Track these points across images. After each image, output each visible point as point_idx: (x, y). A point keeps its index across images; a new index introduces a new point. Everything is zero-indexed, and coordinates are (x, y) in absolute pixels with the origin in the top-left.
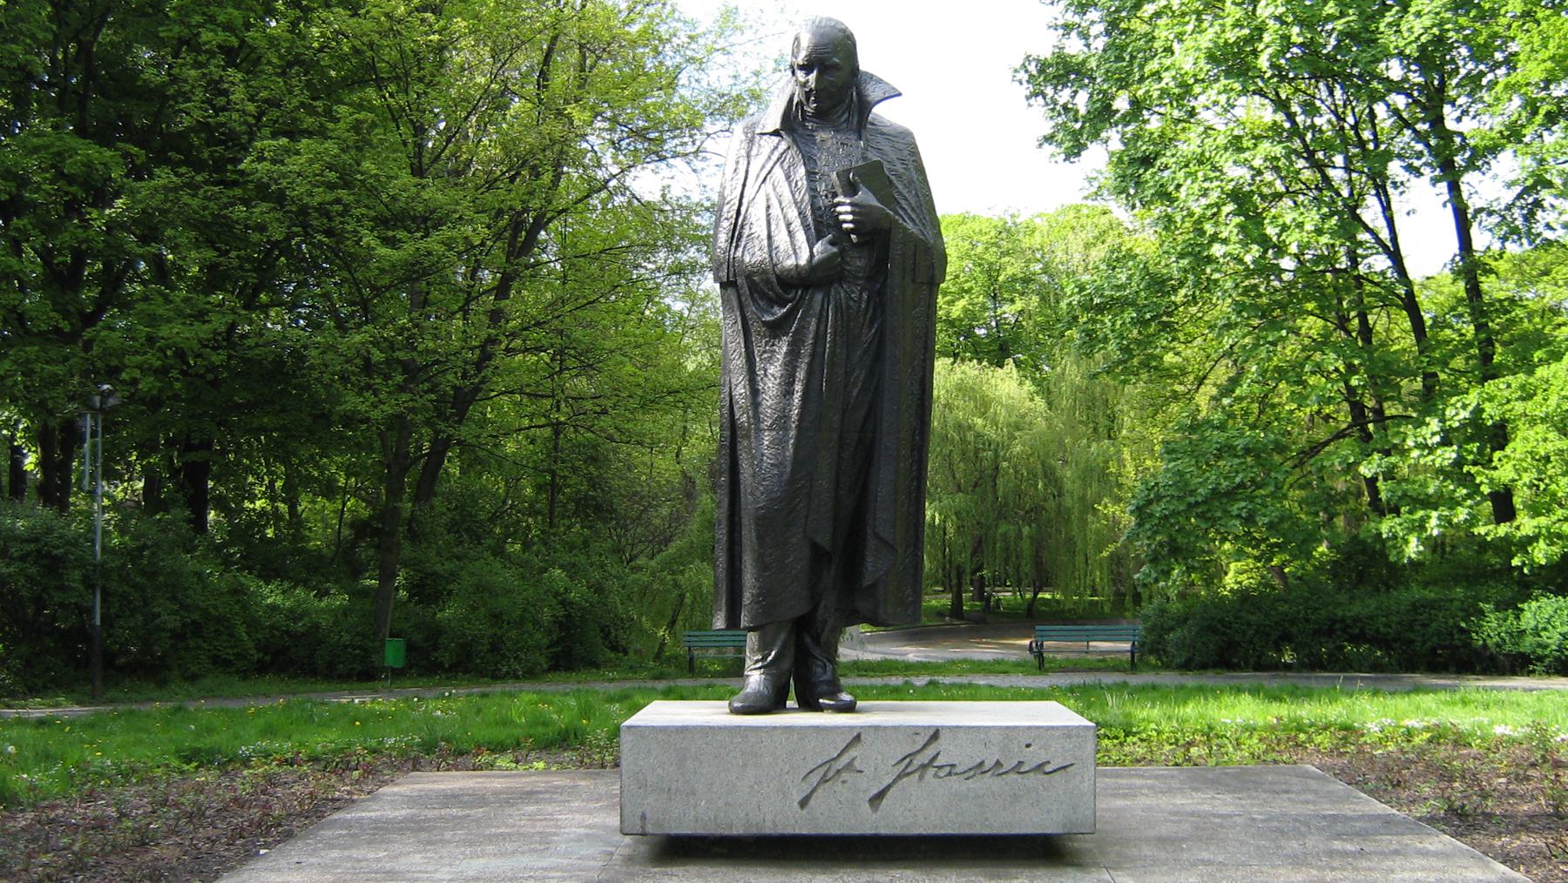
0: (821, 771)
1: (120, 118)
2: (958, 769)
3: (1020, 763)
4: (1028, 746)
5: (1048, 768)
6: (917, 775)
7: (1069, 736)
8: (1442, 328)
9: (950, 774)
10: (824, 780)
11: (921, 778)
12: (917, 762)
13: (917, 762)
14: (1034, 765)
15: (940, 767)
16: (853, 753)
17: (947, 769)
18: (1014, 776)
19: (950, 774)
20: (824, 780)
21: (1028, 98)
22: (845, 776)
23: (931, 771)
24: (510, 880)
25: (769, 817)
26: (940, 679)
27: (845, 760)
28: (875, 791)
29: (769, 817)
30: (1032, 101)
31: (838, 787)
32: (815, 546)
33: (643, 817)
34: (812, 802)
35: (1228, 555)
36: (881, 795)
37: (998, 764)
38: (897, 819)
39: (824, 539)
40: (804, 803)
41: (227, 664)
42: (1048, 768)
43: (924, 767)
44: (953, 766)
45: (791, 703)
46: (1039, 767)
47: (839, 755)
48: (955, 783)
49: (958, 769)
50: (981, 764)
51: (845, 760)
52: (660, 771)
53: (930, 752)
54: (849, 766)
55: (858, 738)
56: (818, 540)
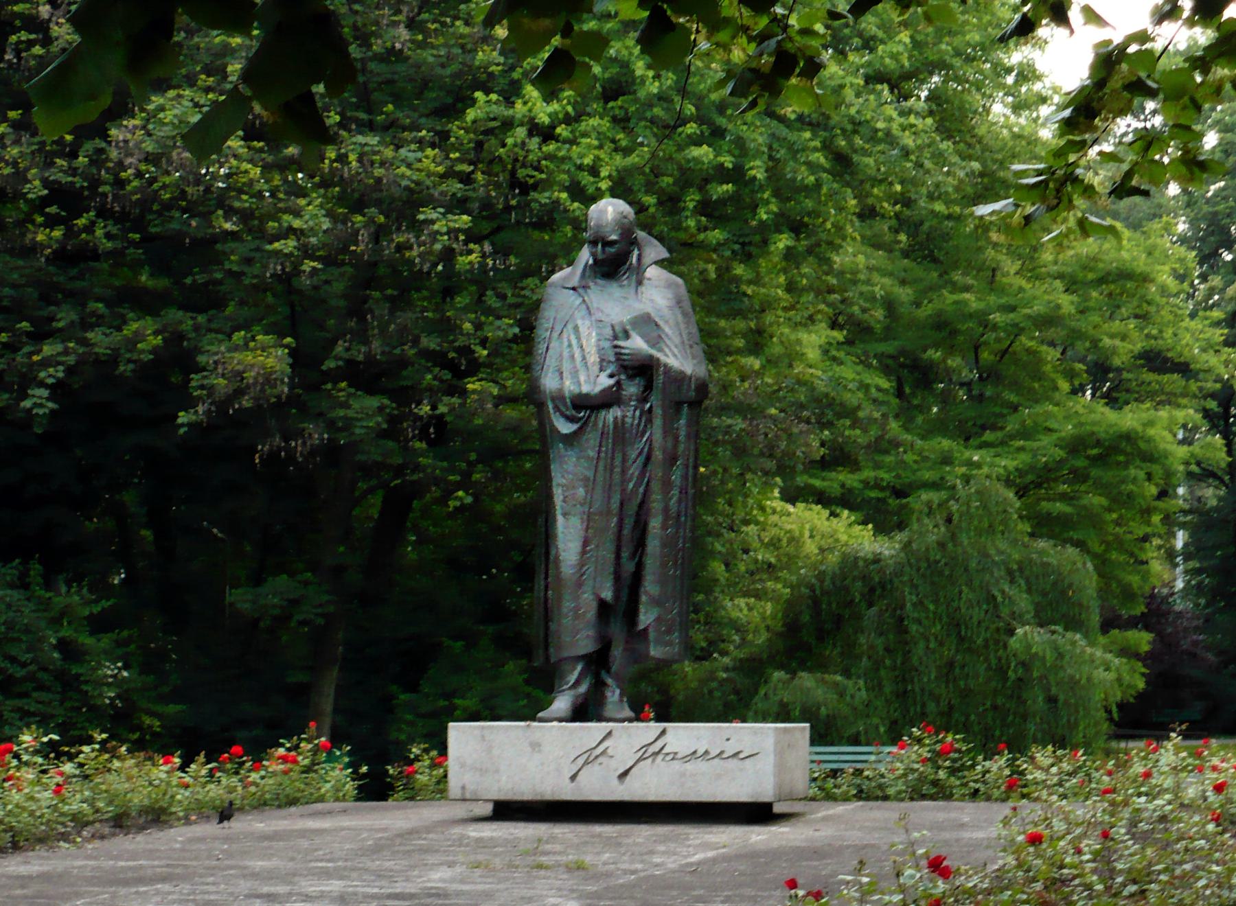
0: (586, 756)
2: (679, 756)
3: (722, 752)
5: (742, 756)
10: (586, 763)
11: (653, 761)
12: (652, 750)
13: (652, 750)
17: (671, 756)
20: (586, 763)
22: (600, 760)
23: (660, 757)
28: (621, 771)
33: (463, 788)
34: (578, 778)
37: (707, 752)
39: (607, 595)
40: (573, 778)
42: (742, 756)
43: (656, 754)
46: (736, 755)
49: (679, 756)
50: (695, 752)
53: (659, 744)
54: (604, 753)
55: (610, 733)
56: (603, 595)
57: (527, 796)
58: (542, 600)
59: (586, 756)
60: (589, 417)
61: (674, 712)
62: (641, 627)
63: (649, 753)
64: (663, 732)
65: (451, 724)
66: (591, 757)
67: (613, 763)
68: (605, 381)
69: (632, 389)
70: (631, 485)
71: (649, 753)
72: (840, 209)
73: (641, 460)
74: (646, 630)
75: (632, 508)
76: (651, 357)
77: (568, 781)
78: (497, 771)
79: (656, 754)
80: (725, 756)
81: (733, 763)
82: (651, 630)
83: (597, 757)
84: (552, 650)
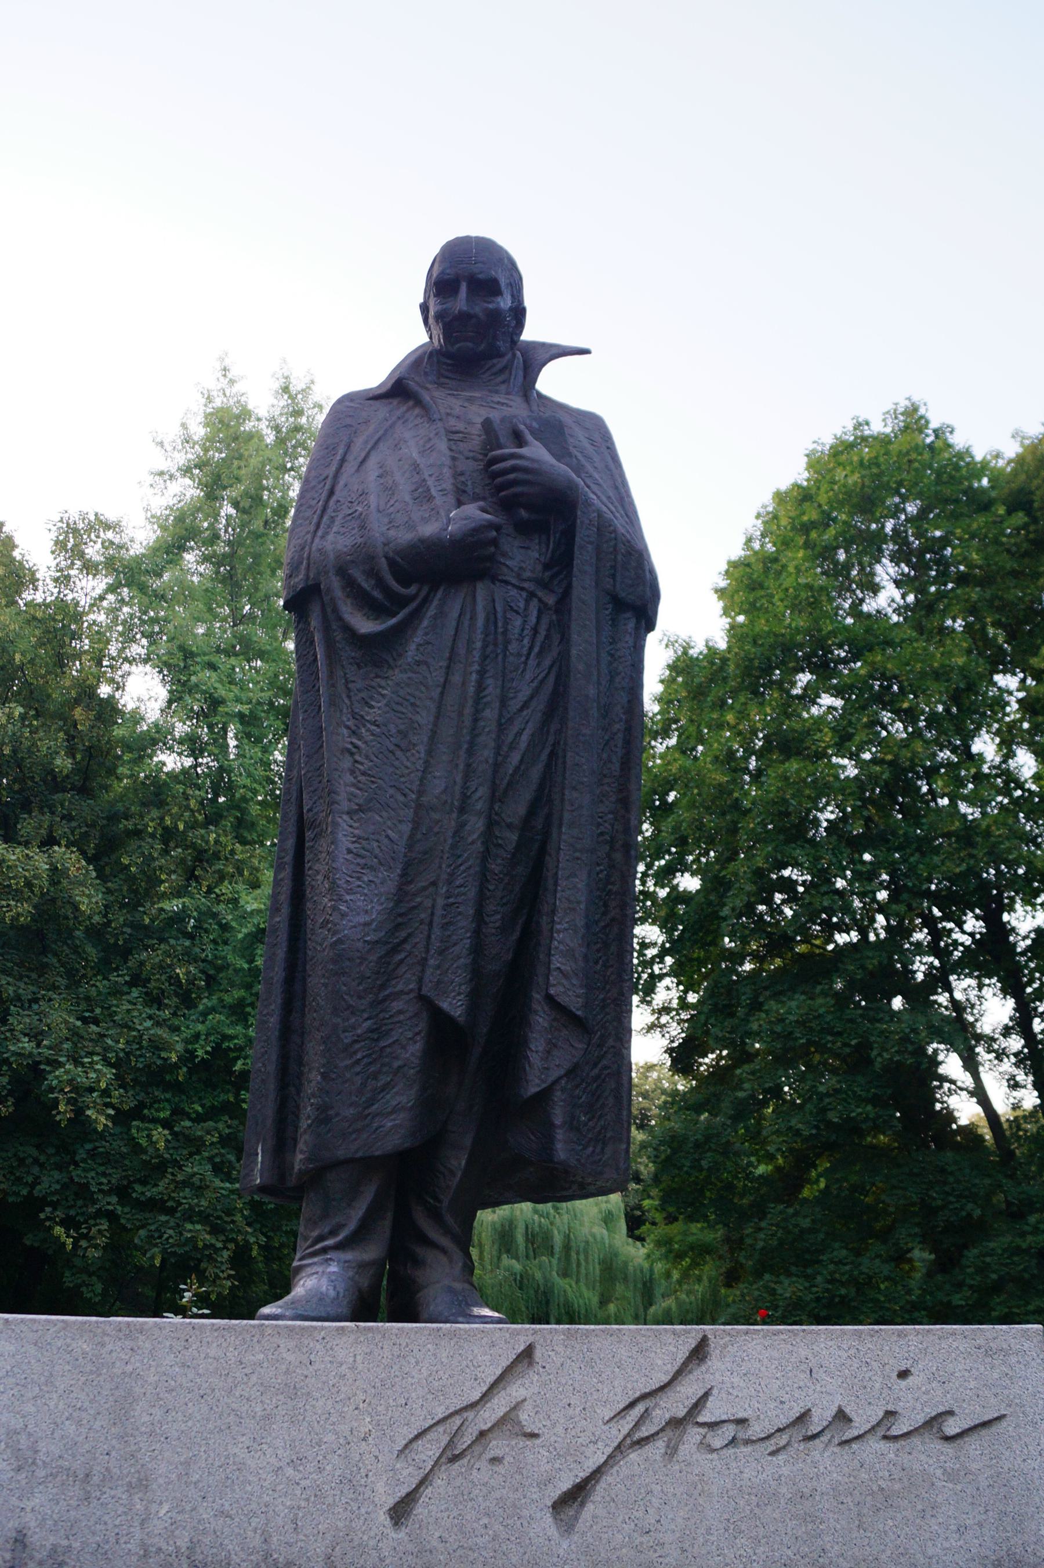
1: (1019, 533)
4: (903, 1374)
5: (952, 1427)
6: (660, 1445)
9: (733, 1442)
10: (451, 1456)
11: (671, 1451)
12: (674, 1404)
14: (920, 1419)
15: (712, 1426)
16: (516, 1391)
17: (729, 1431)
18: (875, 1445)
19: (733, 1442)
20: (451, 1456)
21: (313, 382)
22: (497, 1446)
23: (694, 1435)
26: (500, 630)
27: (498, 1406)
28: (565, 1484)
30: (307, 380)
31: (481, 1472)
32: (438, 1019)
34: (420, 1510)
35: (1021, 720)
36: (577, 1495)
37: (842, 1417)
39: (454, 1005)
43: (676, 1423)
44: (741, 1422)
46: (934, 1422)
47: (485, 1397)
48: (752, 1467)
49: (756, 1430)
50: (803, 1418)
51: (498, 1406)
52: (70, 1428)
53: (688, 1390)
60: (426, 601)
61: (554, 1313)
62: (533, 1088)
64: (699, 1353)
65: (426, 339)
67: (537, 1458)
69: (522, 558)
70: (515, 758)
73: (539, 705)
74: (544, 1096)
75: (516, 809)
76: (570, 481)
77: (383, 1518)
78: (142, 1484)
81: (928, 1455)
82: (558, 1095)
84: (391, 886)
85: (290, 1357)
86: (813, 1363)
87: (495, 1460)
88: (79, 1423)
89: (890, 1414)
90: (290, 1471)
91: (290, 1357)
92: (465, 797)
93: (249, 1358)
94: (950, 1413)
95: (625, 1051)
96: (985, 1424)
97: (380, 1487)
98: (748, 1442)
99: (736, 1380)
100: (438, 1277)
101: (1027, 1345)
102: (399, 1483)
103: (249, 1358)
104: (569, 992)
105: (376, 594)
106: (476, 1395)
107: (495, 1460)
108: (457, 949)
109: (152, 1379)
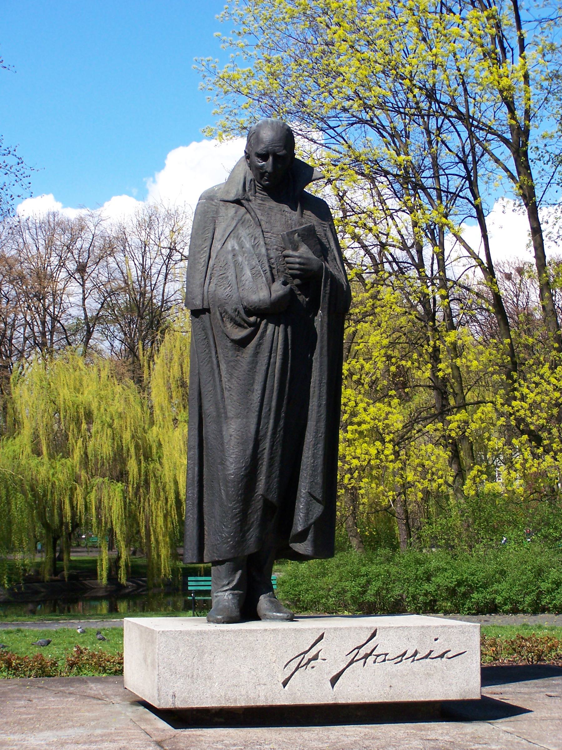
4: (436, 640)
5: (450, 655)
7: (463, 633)
8: (121, 587)
9: (384, 661)
12: (363, 652)
13: (363, 652)
15: (378, 656)
19: (384, 661)
23: (371, 659)
24: (5, 408)
25: (262, 694)
28: (335, 673)
29: (262, 694)
37: (416, 653)
38: (350, 692)
40: (285, 684)
41: (205, 633)
42: (450, 655)
43: (366, 656)
44: (386, 654)
45: (57, 611)
53: (371, 645)
54: (315, 658)
57: (242, 703)
58: (161, 293)
59: (333, 147)
63: (362, 655)
66: (306, 660)
68: (278, 289)
71: (362, 655)
72: (429, 345)
78: (210, 678)
79: (366, 656)
80: (432, 655)
83: (310, 661)
85: (251, 639)
86: (409, 636)
87: (313, 667)
88: (188, 661)
89: (431, 651)
90: (253, 672)
91: (251, 639)
92: (500, 39)
93: (238, 640)
94: (449, 651)
95: (213, 711)
96: (200, 394)
97: (280, 676)
98: (388, 660)
99: (385, 642)
100: (263, 602)
101: (475, 630)
102: (285, 674)
103: (238, 640)
104: (383, 644)
105: (237, 319)
106: (307, 649)
107: (313, 667)
108: (274, 475)
109: (209, 647)
